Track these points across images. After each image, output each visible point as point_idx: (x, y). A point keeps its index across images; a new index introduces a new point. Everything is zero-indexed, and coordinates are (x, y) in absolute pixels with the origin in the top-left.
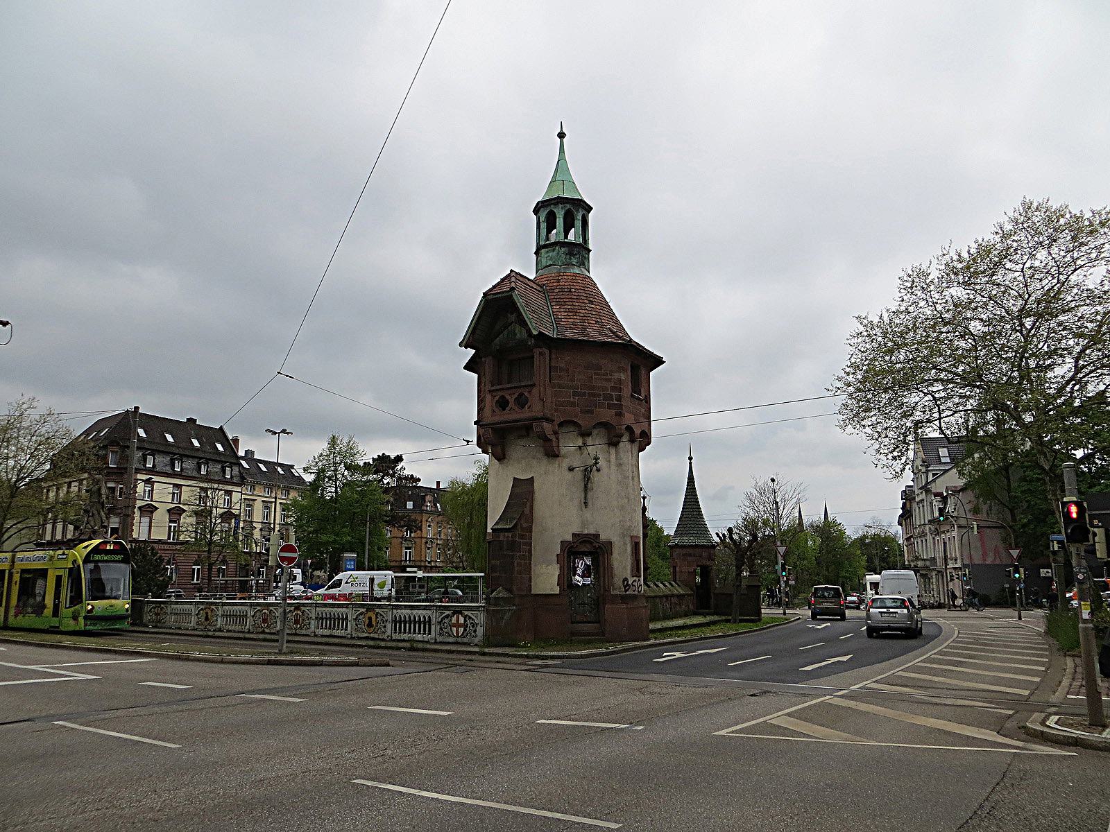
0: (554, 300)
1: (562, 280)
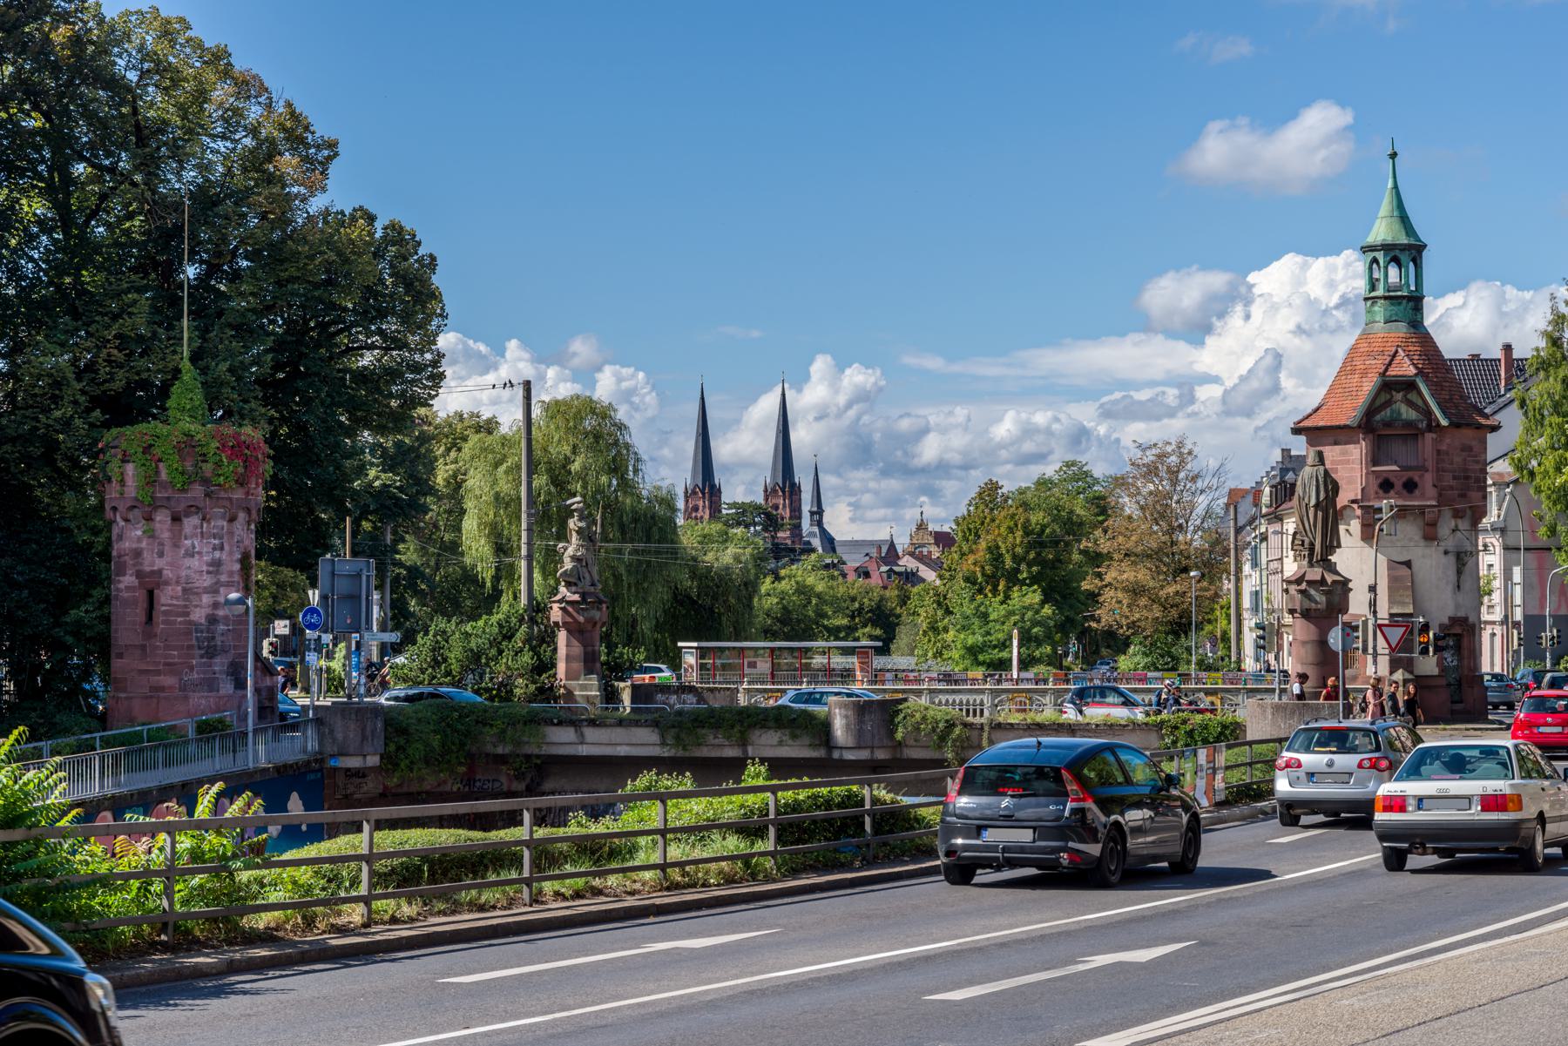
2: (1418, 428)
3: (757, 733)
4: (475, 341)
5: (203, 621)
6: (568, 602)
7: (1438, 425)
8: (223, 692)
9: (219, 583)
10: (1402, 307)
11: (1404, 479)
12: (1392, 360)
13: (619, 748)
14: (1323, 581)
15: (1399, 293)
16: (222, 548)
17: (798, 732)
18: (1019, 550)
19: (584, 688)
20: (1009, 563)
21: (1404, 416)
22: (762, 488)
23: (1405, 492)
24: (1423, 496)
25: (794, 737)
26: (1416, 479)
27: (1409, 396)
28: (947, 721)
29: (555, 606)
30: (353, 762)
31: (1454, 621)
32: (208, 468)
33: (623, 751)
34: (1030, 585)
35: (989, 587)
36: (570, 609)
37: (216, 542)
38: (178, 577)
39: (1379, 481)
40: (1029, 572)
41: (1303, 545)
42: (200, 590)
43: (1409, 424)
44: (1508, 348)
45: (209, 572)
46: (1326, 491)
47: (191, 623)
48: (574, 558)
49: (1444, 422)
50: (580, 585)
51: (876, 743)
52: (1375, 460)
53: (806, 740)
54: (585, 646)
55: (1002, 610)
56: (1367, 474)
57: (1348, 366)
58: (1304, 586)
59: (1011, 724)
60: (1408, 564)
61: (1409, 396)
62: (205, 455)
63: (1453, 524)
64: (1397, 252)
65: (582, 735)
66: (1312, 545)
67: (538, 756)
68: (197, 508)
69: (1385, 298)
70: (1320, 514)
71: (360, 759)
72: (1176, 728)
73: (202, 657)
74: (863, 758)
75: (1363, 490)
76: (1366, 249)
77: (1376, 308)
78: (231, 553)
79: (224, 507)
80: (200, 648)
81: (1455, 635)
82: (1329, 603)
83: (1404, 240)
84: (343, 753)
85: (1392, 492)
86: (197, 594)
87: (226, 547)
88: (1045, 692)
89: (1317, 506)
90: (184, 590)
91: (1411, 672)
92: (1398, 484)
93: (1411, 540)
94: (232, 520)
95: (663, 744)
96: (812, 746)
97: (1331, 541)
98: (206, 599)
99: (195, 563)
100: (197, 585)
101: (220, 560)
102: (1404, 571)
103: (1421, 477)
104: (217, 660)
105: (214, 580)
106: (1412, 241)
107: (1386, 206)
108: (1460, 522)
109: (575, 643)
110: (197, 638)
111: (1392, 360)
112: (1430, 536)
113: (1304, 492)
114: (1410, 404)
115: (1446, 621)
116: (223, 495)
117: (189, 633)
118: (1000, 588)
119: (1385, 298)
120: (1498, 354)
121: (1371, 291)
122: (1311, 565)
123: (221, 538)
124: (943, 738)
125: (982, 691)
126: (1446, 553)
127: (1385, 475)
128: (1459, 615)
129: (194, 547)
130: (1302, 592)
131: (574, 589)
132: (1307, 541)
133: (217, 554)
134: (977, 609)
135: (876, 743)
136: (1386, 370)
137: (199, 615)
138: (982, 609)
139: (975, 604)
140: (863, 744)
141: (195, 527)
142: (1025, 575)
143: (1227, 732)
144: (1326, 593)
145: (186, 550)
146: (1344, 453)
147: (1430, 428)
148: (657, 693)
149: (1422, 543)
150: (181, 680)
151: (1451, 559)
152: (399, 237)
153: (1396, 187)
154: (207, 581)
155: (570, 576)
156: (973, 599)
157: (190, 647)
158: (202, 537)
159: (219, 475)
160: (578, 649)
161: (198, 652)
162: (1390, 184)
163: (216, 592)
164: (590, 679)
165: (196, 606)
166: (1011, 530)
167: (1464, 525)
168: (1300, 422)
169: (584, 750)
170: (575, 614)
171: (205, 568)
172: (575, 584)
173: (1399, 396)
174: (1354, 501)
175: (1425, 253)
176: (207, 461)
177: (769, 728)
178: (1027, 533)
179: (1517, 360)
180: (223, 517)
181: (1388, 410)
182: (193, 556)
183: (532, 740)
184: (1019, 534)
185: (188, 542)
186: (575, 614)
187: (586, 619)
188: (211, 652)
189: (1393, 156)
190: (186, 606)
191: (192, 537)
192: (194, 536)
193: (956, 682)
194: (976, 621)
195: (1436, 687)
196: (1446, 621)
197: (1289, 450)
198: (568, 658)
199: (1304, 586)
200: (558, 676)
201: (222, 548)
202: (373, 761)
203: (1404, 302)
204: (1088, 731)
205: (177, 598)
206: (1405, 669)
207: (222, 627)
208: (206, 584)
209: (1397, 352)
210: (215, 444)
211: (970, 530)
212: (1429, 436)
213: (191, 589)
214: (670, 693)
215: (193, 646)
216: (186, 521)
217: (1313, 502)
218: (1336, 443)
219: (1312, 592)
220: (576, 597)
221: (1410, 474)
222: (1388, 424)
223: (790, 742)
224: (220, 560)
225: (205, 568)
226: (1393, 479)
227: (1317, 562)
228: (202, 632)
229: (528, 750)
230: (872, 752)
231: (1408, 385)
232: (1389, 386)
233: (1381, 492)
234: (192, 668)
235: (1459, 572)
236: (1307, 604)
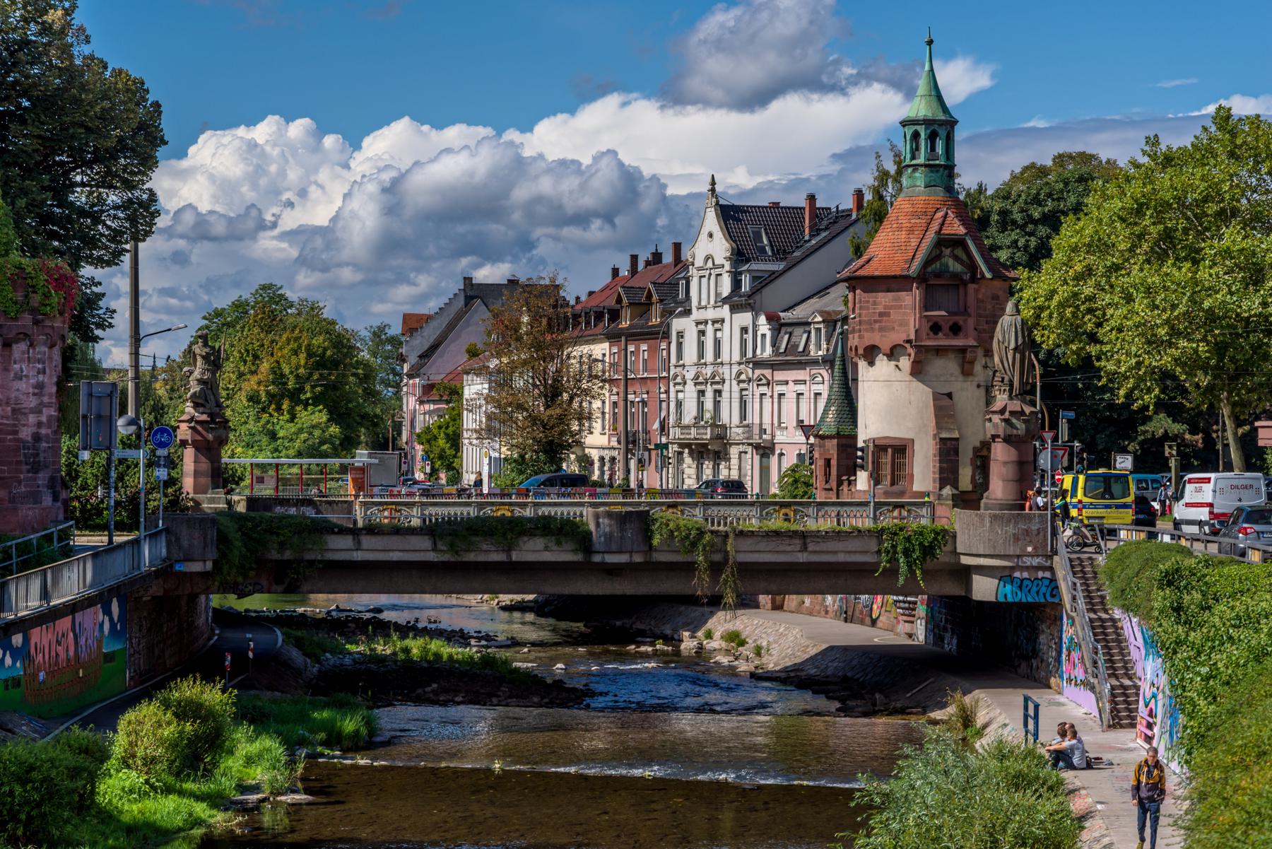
2: (962, 280)
3: (526, 539)
5: (29, 439)
6: (197, 422)
7: (983, 276)
8: (44, 504)
9: (41, 404)
10: (939, 174)
11: (951, 323)
12: (944, 221)
13: (391, 554)
14: (1022, 413)
15: (937, 162)
16: (44, 373)
17: (563, 540)
18: (301, 371)
19: (212, 501)
20: (291, 384)
21: (951, 269)
23: (951, 334)
24: (966, 337)
25: (559, 543)
26: (961, 323)
27: (956, 252)
28: (698, 529)
29: (184, 426)
30: (196, 567)
32: (36, 299)
33: (396, 556)
34: (315, 405)
35: (273, 406)
36: (199, 428)
37: (40, 366)
38: (8, 398)
39: (930, 324)
40: (312, 392)
41: (1002, 381)
42: (27, 411)
43: (956, 276)
44: (812, 198)
45: (34, 394)
46: (1023, 336)
47: (19, 440)
48: (200, 381)
49: (988, 275)
50: (208, 406)
51: (635, 548)
52: (927, 306)
53: (569, 546)
54: (212, 462)
55: (292, 428)
56: (920, 317)
59: (752, 532)
60: (950, 395)
61: (956, 252)
62: (33, 286)
64: (936, 127)
65: (359, 543)
66: (1011, 382)
67: (320, 562)
68: (25, 334)
69: (926, 166)
70: (1018, 356)
71: (201, 564)
72: (895, 534)
73: (28, 471)
74: (624, 561)
75: (916, 331)
77: (917, 174)
78: (51, 376)
79: (46, 334)
80: (27, 464)
82: (1027, 430)
83: (942, 117)
84: (188, 559)
85: (940, 334)
86: (25, 414)
87: (48, 371)
88: (413, 504)
89: (1015, 349)
90: (14, 410)
91: (957, 488)
92: (946, 328)
93: (952, 375)
94: (52, 347)
95: (435, 549)
96: (575, 551)
98: (32, 419)
99: (22, 385)
100: (24, 406)
101: (43, 383)
102: (946, 402)
103: (965, 321)
104: (40, 475)
105: (38, 402)
109: (203, 459)
110: (25, 454)
111: (944, 221)
112: (967, 372)
113: (1004, 337)
114: (957, 258)
115: (978, 444)
116: (48, 323)
117: (18, 449)
118: (284, 407)
119: (926, 166)
120: (799, 200)
122: (1011, 398)
123: (44, 363)
124: (694, 545)
125: (582, 504)
126: (979, 386)
127: (935, 319)
129: (22, 371)
130: (1006, 421)
131: (201, 409)
132: (1006, 379)
133: (41, 377)
134: (264, 427)
135: (635, 548)
136: (941, 229)
137: (26, 433)
138: (269, 426)
139: (263, 421)
140: (624, 550)
141: (23, 353)
142: (308, 395)
143: (939, 538)
144: (1025, 421)
145: (16, 374)
146: (895, 300)
147: (974, 279)
148: (276, 505)
149: (961, 378)
150: (10, 493)
151: (982, 391)
152: (137, 90)
154: (33, 402)
155: (199, 397)
156: (258, 419)
157: (18, 463)
158: (29, 361)
159: (46, 305)
160: (205, 465)
161: (25, 468)
162: (927, 67)
163: (40, 412)
164: (217, 493)
165: (24, 425)
166: (295, 352)
168: (855, 272)
169: (359, 556)
170: (204, 432)
171: (31, 390)
172: (203, 405)
173: (947, 251)
176: (36, 292)
177: (535, 535)
178: (310, 355)
179: (819, 209)
180: (45, 344)
181: (938, 264)
182: (21, 379)
183: (315, 547)
184: (303, 356)
185: (17, 366)
186: (204, 432)
187: (214, 437)
188: (36, 468)
189: (930, 43)
190: (15, 425)
191: (20, 362)
192: (22, 360)
193: (434, 496)
194: (265, 440)
196: (978, 444)
197: (471, 279)
198: (197, 474)
200: (184, 490)
201: (44, 373)
202: (209, 566)
204: (818, 537)
205: (7, 418)
206: (952, 486)
207: (44, 445)
208: (32, 405)
209: (947, 213)
210: (43, 277)
211: (247, 351)
212: (972, 287)
213: (19, 409)
214: (290, 506)
215: (21, 462)
216: (14, 346)
217: (1012, 345)
218: (888, 291)
219: (1014, 421)
220: (204, 417)
221: (956, 318)
222: (938, 275)
223: (556, 548)
224: (43, 383)
225: (31, 390)
226: (942, 323)
227: (1016, 395)
228: (29, 449)
229: (310, 556)
230: (631, 557)
231: (958, 242)
232: (944, 243)
233: (931, 333)
234: (20, 482)
236: (1010, 431)
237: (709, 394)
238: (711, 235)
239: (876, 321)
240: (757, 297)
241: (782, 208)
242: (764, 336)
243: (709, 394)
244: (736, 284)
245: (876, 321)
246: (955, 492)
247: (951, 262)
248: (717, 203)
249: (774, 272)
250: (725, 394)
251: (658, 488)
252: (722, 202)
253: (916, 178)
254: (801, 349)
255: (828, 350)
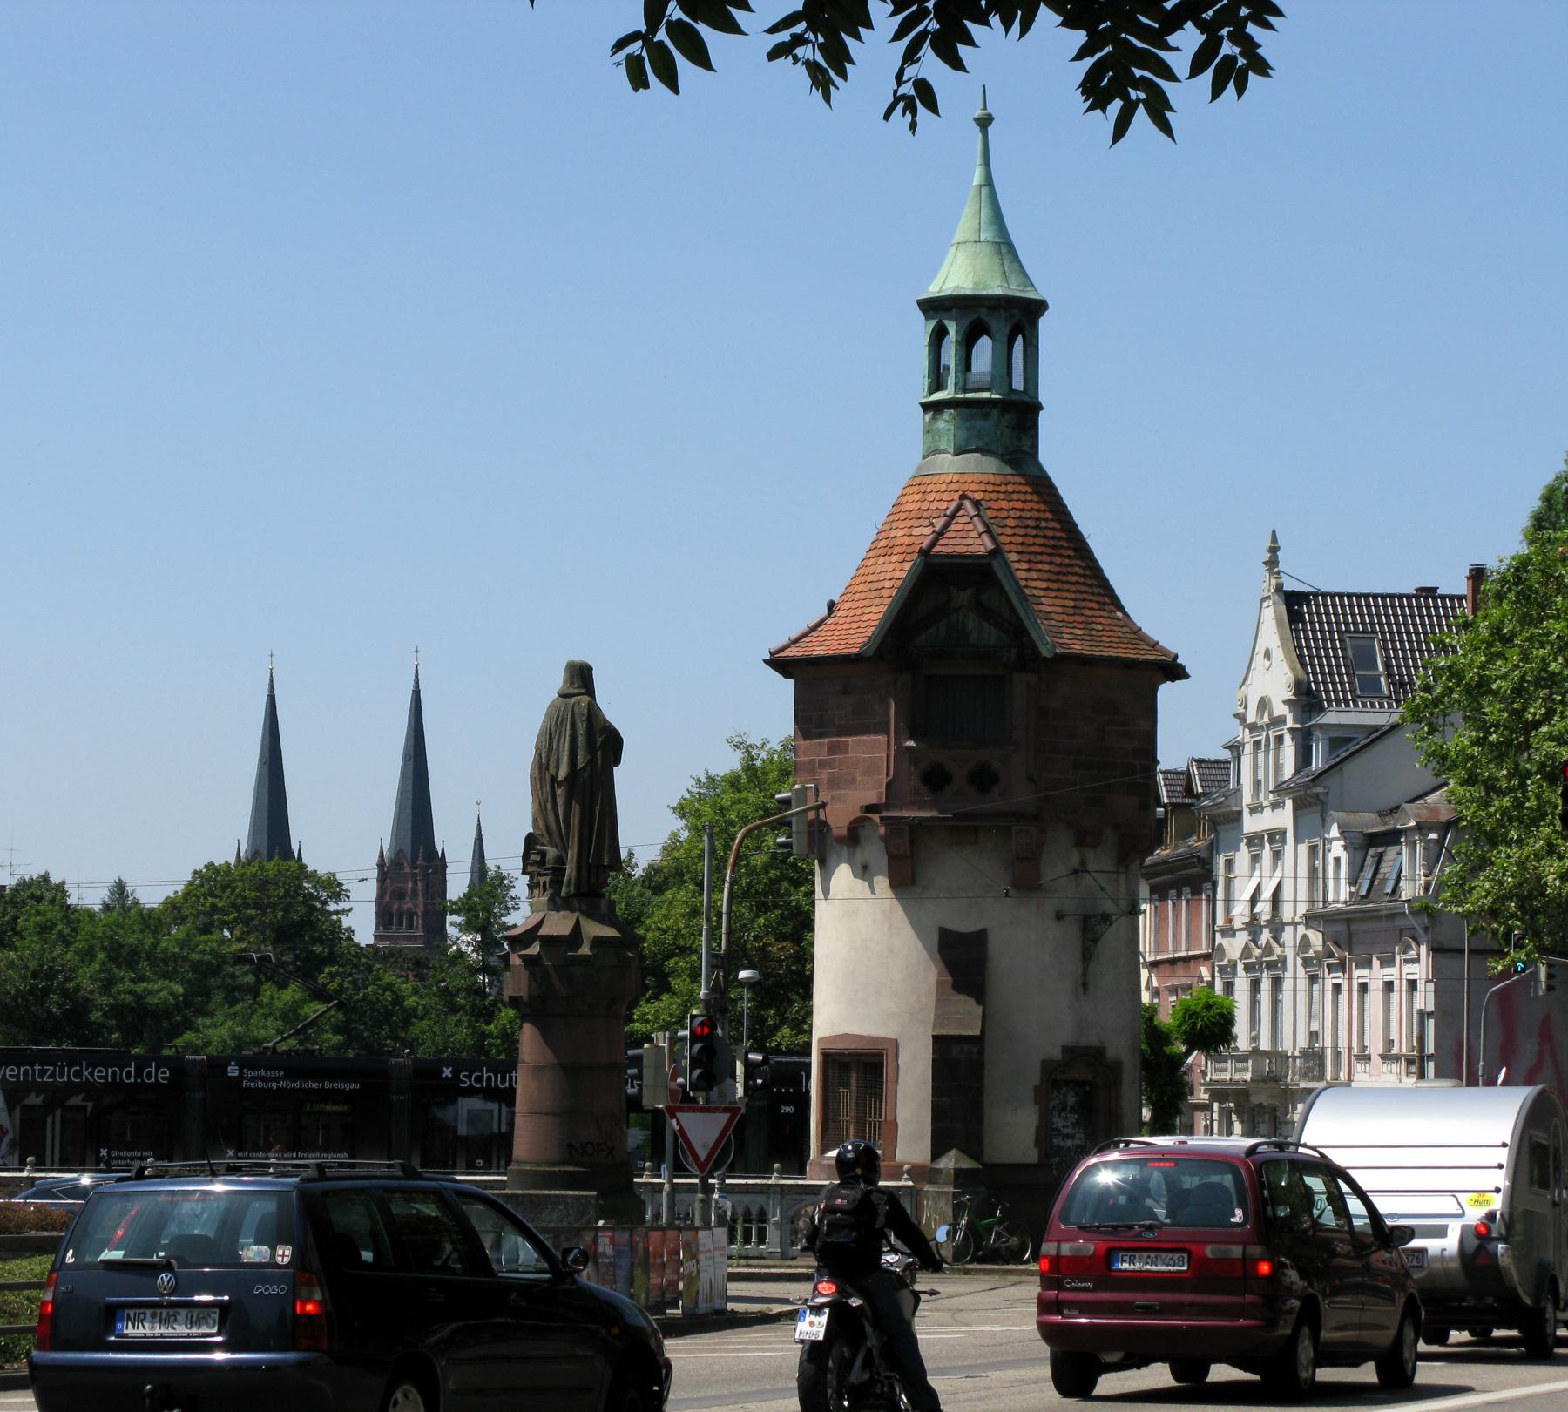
0: (1013, 547)
1: (1015, 496)
4: (1151, 854)
22: (376, 859)
31: (1074, 1054)
57: (881, 548)
58: (535, 949)
63: (1075, 859)
64: (983, 313)
76: (931, 307)
77: (941, 424)
81: (1080, 1084)
91: (976, 1155)
97: (599, 856)
106: (1014, 290)
107: (968, 221)
108: (1090, 855)
114: (986, 613)
115: (1056, 1054)
121: (931, 391)
126: (1060, 916)
128: (1084, 1042)
151: (1072, 930)
153: (989, 182)
162: (977, 177)
167: (1101, 861)
173: (963, 597)
174: (871, 809)
175: (1044, 323)
189: (984, 122)
195: (531, 1163)
199: (535, 949)
203: (995, 412)
235: (1087, 956)
237: (1266, 985)
238: (1267, 655)
239: (823, 764)
240: (1333, 781)
241: (1443, 597)
242: (1337, 860)
243: (1266, 985)
244: (1304, 757)
245: (823, 764)
246: (967, 1164)
247: (972, 621)
248: (1279, 589)
249: (1375, 728)
250: (1287, 985)
251: (496, 1129)
252: (1290, 585)
253: (938, 432)
254: (1389, 890)
255: (1427, 889)
